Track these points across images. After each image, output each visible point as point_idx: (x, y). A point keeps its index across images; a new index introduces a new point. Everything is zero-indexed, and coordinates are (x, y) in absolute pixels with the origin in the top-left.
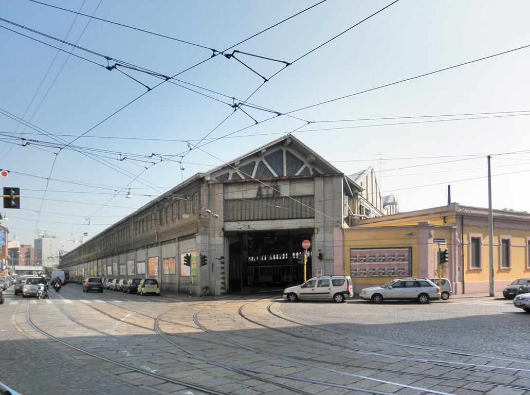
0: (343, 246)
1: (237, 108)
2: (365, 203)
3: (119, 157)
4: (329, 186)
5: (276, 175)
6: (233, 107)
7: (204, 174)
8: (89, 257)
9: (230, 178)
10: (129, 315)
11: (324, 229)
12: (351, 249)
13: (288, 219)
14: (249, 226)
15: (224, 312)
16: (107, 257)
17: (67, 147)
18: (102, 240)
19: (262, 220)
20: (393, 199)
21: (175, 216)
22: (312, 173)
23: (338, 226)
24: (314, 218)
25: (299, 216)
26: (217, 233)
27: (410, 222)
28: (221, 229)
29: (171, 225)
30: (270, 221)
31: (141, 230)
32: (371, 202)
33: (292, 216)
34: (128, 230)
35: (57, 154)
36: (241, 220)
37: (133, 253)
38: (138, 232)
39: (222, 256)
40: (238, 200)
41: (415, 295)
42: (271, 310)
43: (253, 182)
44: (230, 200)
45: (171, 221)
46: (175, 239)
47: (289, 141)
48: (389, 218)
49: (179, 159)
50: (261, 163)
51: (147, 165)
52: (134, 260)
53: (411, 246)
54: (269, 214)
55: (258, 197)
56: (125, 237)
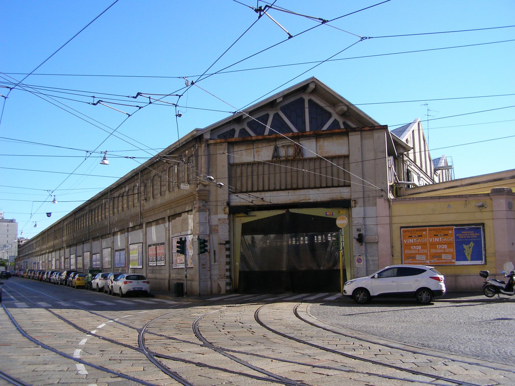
0: (391, 224)
1: (262, 13)
2: (412, 167)
3: (91, 100)
4: (369, 143)
5: (295, 130)
6: (256, 11)
7: (202, 130)
8: (54, 246)
9: (237, 135)
10: (103, 325)
11: (364, 201)
12: (401, 227)
13: (315, 188)
14: (262, 199)
15: (234, 319)
16: (76, 245)
17: (17, 87)
18: (70, 223)
19: (280, 190)
20: (446, 162)
21: (163, 189)
22: (342, 127)
23: (382, 196)
24: (349, 186)
25: (330, 184)
26: (220, 209)
27: (484, 189)
28: (225, 204)
29: (159, 200)
30: (291, 192)
31: (120, 208)
32: (419, 165)
33: (321, 185)
34: (103, 208)
35: (6, 98)
36: (252, 191)
37: (109, 239)
38: (116, 210)
39: (227, 240)
40: (248, 164)
41: (413, 288)
42: (300, 314)
43: (267, 140)
44: (237, 165)
45: (159, 195)
46: (164, 218)
47: (312, 86)
48: (448, 185)
49: (174, 100)
50: (277, 115)
51: (130, 110)
52: (111, 247)
53: (483, 222)
54: (283, 183)
55: (275, 159)
56: (100, 217)
